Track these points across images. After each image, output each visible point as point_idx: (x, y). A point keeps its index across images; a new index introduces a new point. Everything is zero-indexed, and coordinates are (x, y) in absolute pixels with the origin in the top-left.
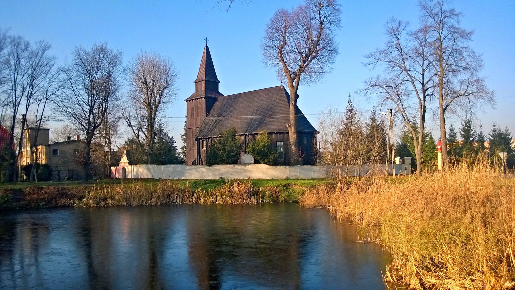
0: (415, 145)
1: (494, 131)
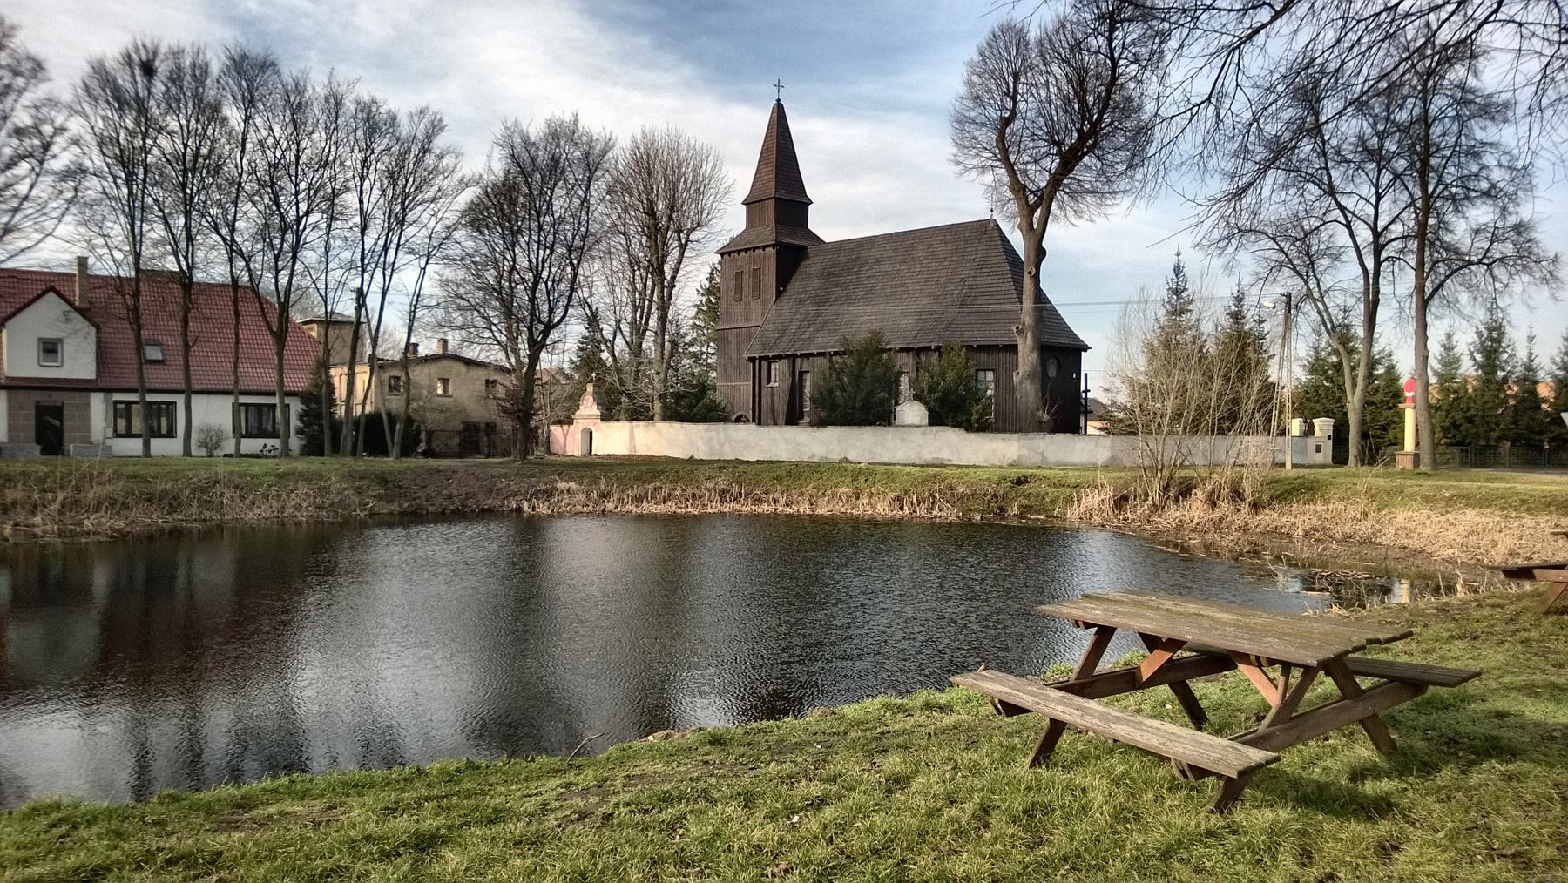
0: (1348, 386)
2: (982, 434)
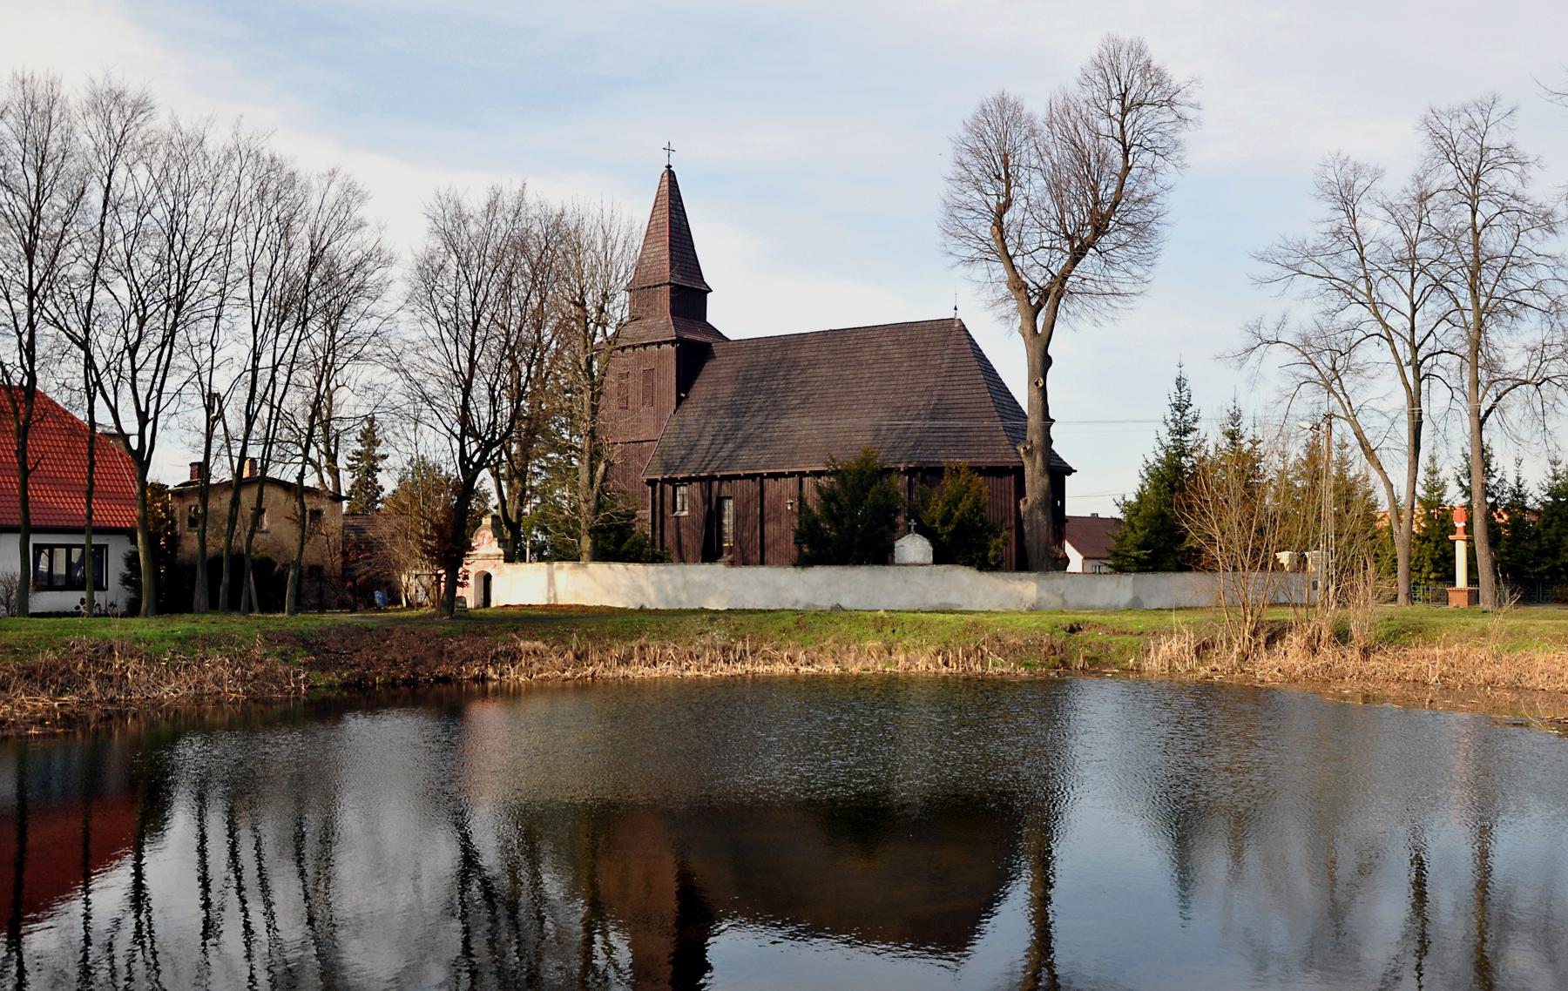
1: (1556, 478)
2: (995, 574)
